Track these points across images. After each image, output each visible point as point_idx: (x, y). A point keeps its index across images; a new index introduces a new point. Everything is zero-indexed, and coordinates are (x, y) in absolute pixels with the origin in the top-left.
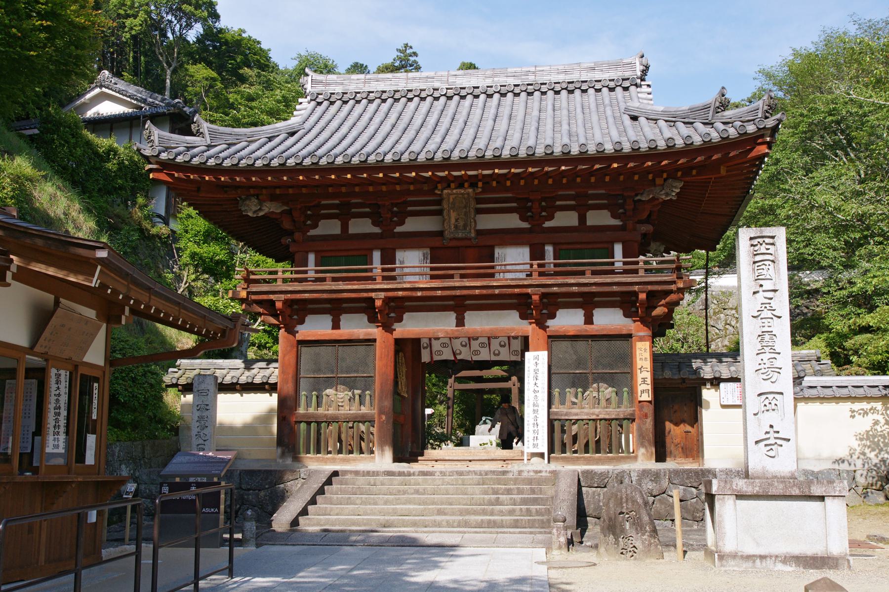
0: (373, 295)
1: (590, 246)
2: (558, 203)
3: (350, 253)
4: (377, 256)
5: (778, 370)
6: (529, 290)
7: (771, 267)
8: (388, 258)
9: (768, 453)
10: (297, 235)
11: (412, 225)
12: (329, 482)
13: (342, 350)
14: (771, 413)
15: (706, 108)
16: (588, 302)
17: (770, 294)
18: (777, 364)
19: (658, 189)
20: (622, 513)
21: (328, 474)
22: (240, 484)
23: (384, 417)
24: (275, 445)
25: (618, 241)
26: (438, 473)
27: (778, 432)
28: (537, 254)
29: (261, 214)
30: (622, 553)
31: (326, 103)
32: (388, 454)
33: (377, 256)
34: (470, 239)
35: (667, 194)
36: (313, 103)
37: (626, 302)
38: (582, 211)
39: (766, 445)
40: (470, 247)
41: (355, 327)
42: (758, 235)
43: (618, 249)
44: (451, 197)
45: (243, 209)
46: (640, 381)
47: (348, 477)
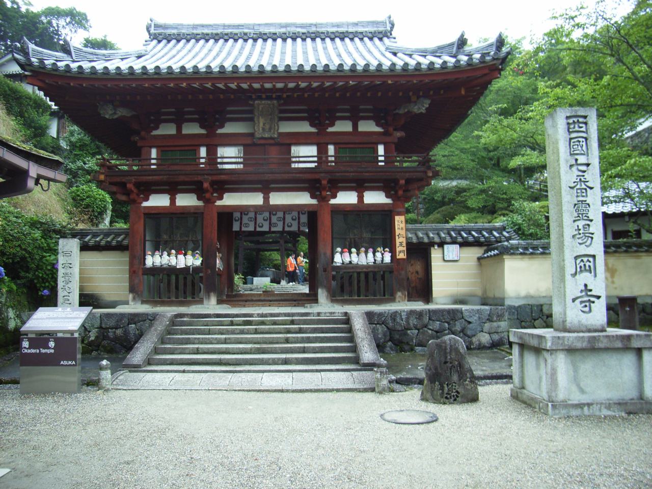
1: (361, 146)
5: (591, 235)
7: (584, 144)
10: (143, 133)
11: (230, 128)
15: (452, 44)
17: (583, 168)
18: (591, 230)
24: (128, 290)
25: (381, 143)
27: (591, 290)
29: (116, 117)
42: (573, 114)
45: (102, 112)
46: (398, 244)
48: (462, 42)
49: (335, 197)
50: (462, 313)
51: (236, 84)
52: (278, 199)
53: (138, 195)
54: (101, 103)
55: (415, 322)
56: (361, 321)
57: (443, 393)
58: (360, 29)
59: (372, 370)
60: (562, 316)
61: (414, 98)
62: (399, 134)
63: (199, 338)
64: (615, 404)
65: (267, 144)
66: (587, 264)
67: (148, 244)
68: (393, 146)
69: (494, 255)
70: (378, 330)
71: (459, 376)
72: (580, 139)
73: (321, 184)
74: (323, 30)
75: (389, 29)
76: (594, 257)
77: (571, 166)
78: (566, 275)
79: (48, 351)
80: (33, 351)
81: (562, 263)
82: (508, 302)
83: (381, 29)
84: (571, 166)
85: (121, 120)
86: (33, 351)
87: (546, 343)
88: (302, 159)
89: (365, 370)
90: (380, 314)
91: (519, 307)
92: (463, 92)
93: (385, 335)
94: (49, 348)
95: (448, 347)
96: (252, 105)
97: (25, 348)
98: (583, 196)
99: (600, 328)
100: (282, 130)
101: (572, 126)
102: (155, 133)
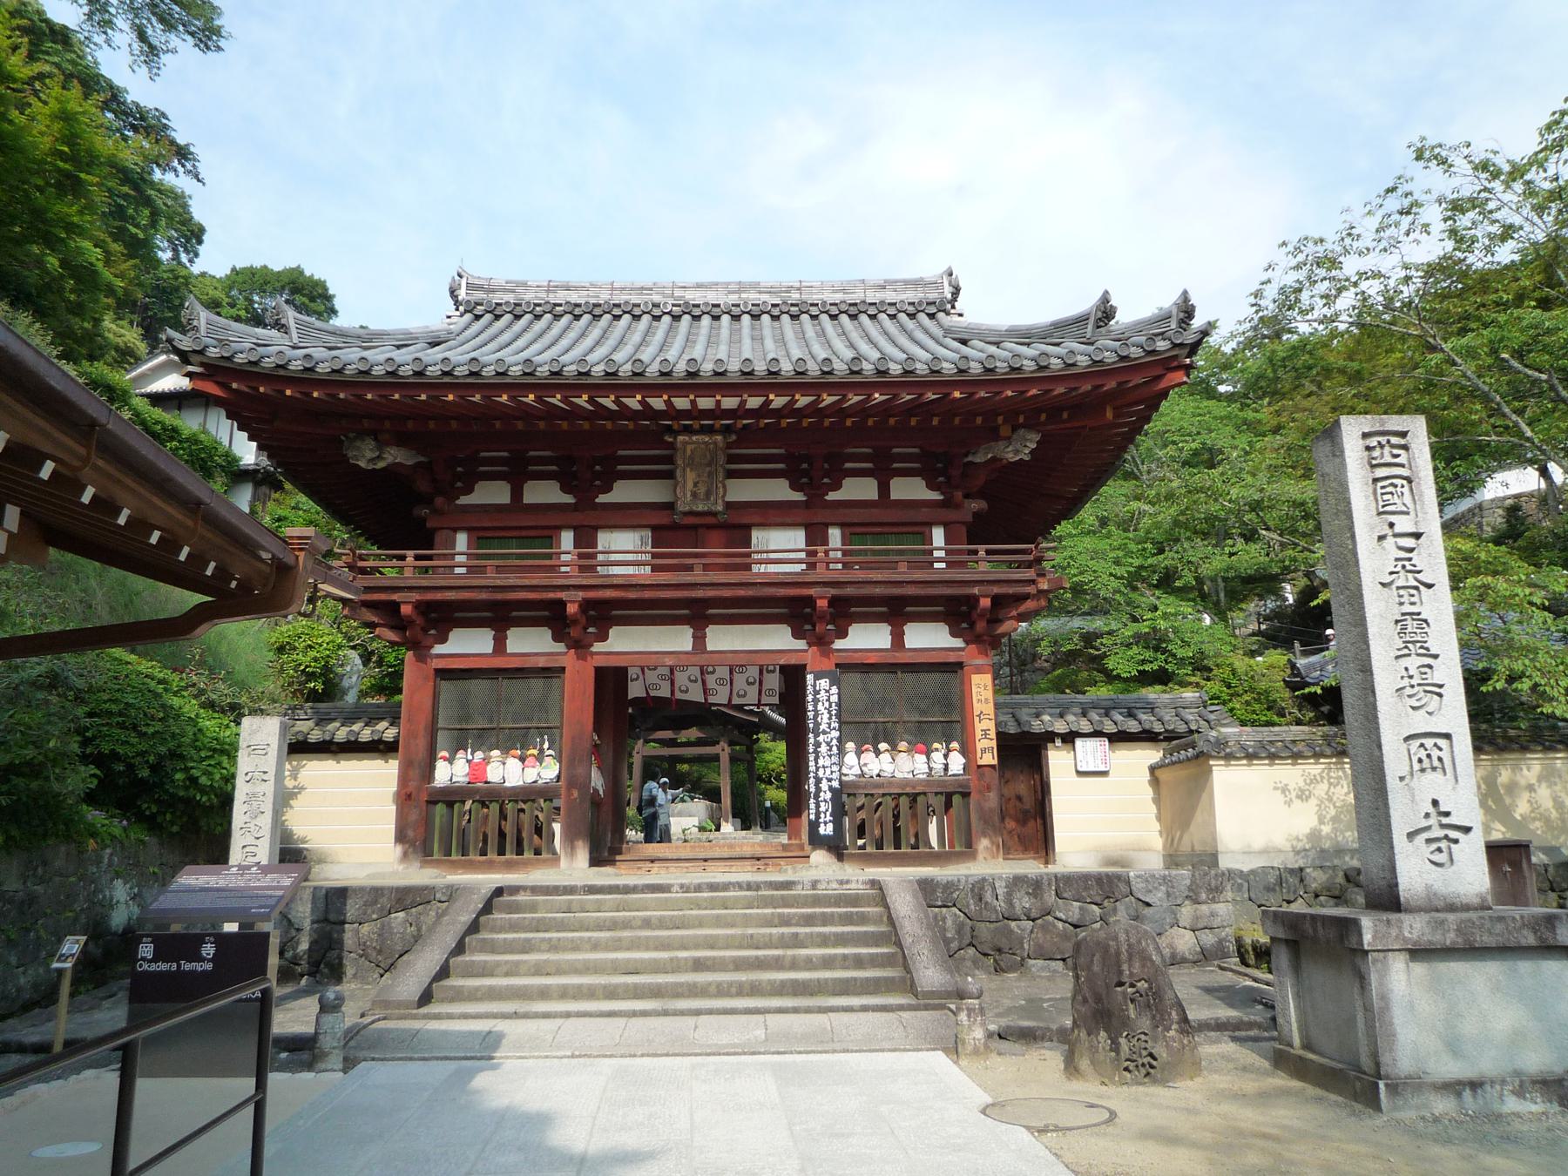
0: (563, 595)
1: (895, 530)
2: (848, 465)
3: (524, 533)
4: (567, 539)
6: (812, 591)
7: (1406, 490)
8: (585, 539)
9: (1433, 858)
10: (439, 501)
11: (624, 492)
12: (488, 908)
13: (505, 684)
14: (1430, 775)
16: (895, 611)
17: (1409, 542)
19: (1001, 444)
20: (1121, 984)
21: (486, 892)
22: (327, 911)
23: (576, 794)
25: (938, 524)
26: (676, 888)
27: (1447, 814)
28: (816, 536)
29: (381, 465)
30: (1126, 1069)
31: (488, 317)
32: (582, 855)
33: (567, 539)
34: (714, 514)
35: (1017, 452)
36: (468, 316)
37: (955, 610)
38: (883, 474)
39: (1429, 841)
40: (709, 527)
41: (530, 643)
42: (1378, 428)
43: (938, 536)
44: (689, 448)
45: (350, 454)
46: (978, 734)
47: (521, 897)
48: (1105, 312)
49: (843, 634)
50: (1128, 883)
51: (639, 397)
52: (723, 639)
53: (425, 630)
54: (351, 435)
55: (1027, 902)
56: (908, 898)
57: (1118, 1058)
58: (890, 296)
59: (943, 1007)
60: (1388, 875)
61: (1005, 431)
62: (976, 505)
63: (550, 939)
64: (1534, 1082)
65: (702, 526)
66: (1435, 753)
67: (442, 737)
68: (964, 529)
69: (1188, 759)
70: (944, 919)
71: (1154, 1017)
72: (1395, 481)
73: (814, 607)
74: (815, 298)
75: (949, 296)
76: (1447, 736)
77: (1381, 538)
78: (1388, 778)
79: (199, 967)
80: (163, 967)
81: (1377, 753)
82: (1225, 863)
83: (932, 296)
84: (1381, 538)
85: (392, 472)
86: (163, 967)
87: (1360, 935)
88: (772, 556)
89: (926, 1008)
90: (949, 886)
91: (1252, 872)
92: (1109, 414)
93: (960, 929)
94: (202, 959)
95: (1124, 948)
96: (672, 446)
97: (144, 959)
98: (1413, 604)
99: (1476, 901)
100: (732, 497)
101: (1376, 453)
102: (464, 500)
